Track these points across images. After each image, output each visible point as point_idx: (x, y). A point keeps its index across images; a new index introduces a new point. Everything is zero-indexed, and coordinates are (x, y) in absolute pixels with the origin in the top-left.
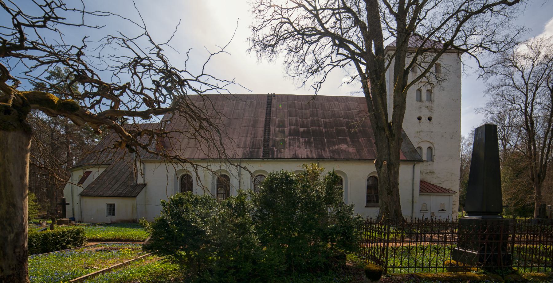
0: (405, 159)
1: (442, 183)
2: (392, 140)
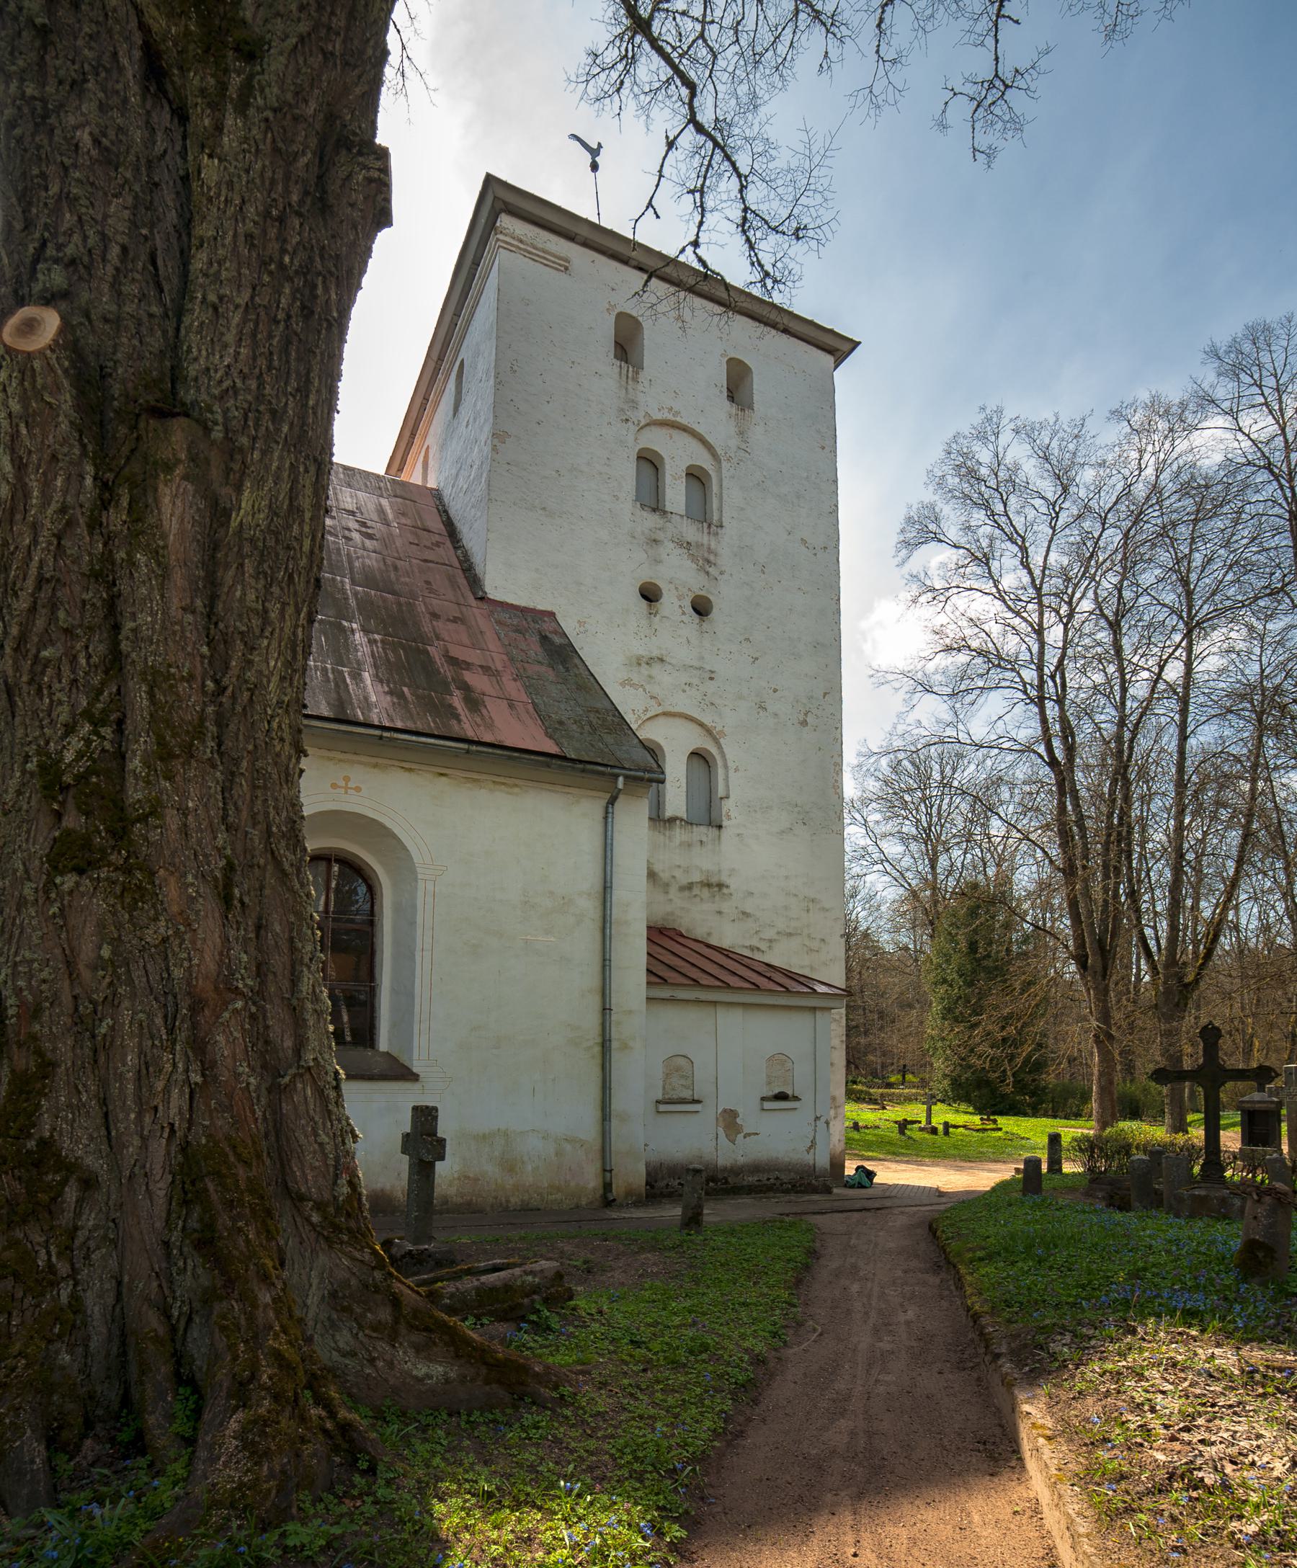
0: (551, 748)
1: (763, 946)
2: (216, 106)
